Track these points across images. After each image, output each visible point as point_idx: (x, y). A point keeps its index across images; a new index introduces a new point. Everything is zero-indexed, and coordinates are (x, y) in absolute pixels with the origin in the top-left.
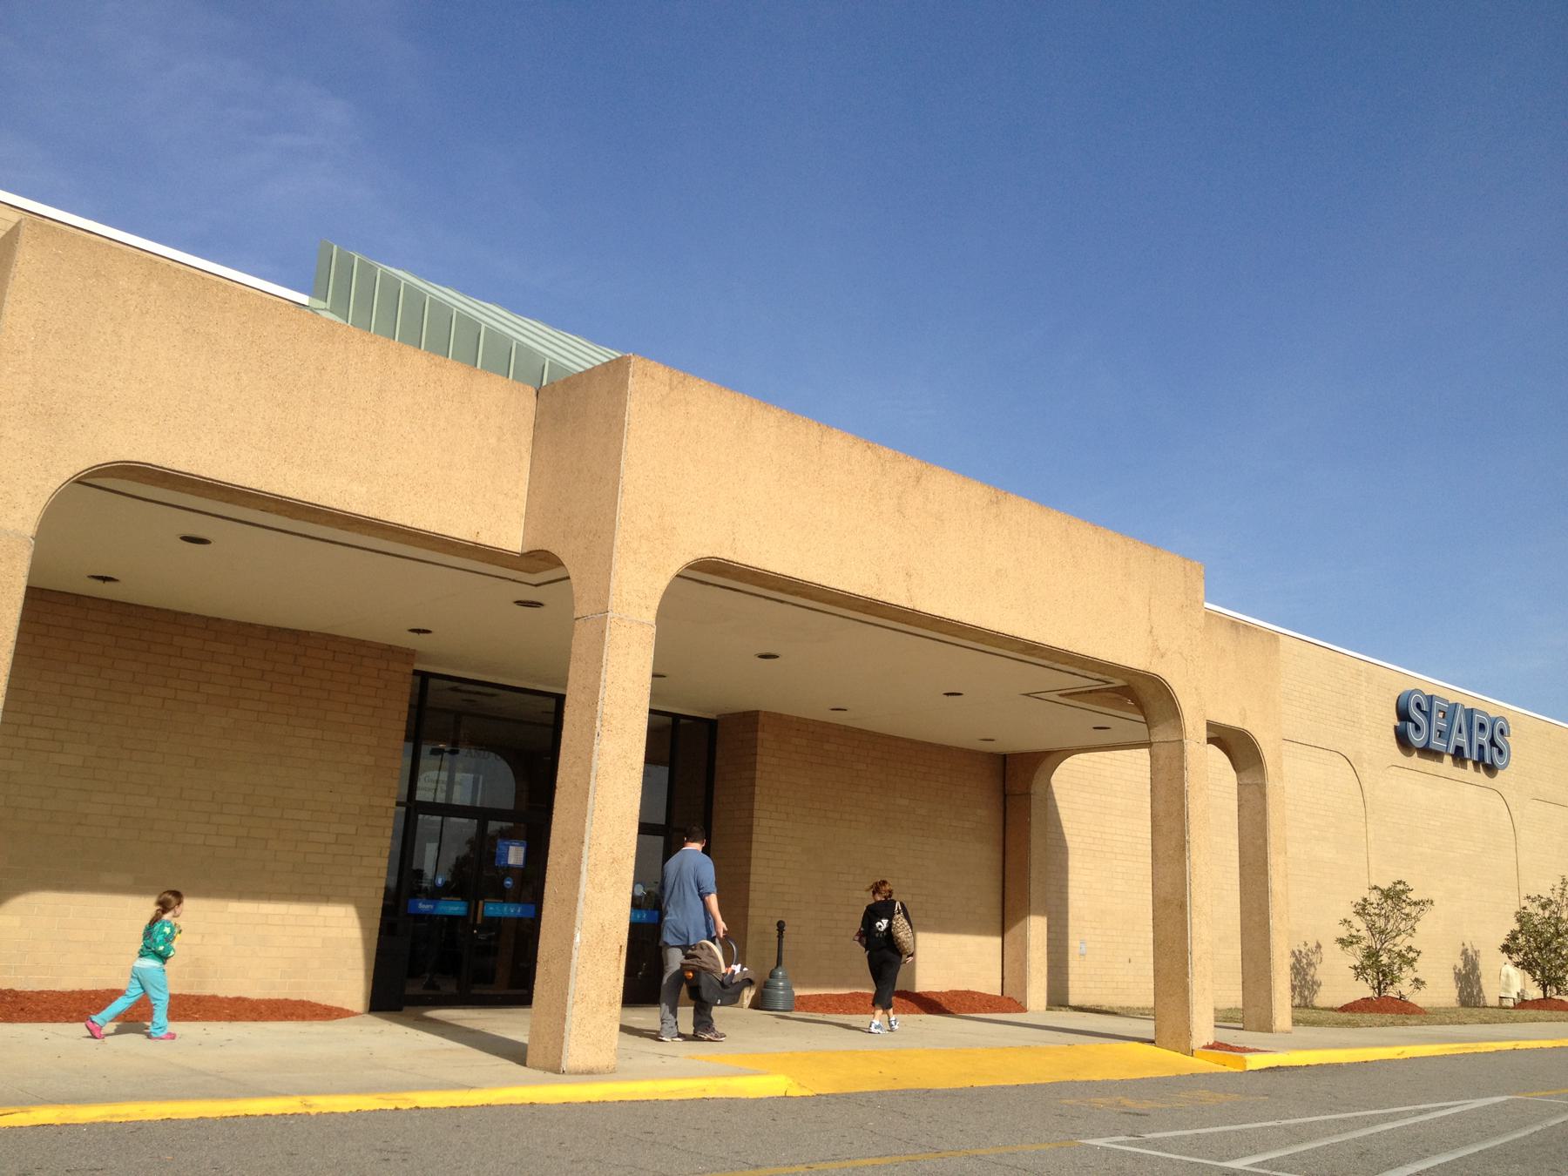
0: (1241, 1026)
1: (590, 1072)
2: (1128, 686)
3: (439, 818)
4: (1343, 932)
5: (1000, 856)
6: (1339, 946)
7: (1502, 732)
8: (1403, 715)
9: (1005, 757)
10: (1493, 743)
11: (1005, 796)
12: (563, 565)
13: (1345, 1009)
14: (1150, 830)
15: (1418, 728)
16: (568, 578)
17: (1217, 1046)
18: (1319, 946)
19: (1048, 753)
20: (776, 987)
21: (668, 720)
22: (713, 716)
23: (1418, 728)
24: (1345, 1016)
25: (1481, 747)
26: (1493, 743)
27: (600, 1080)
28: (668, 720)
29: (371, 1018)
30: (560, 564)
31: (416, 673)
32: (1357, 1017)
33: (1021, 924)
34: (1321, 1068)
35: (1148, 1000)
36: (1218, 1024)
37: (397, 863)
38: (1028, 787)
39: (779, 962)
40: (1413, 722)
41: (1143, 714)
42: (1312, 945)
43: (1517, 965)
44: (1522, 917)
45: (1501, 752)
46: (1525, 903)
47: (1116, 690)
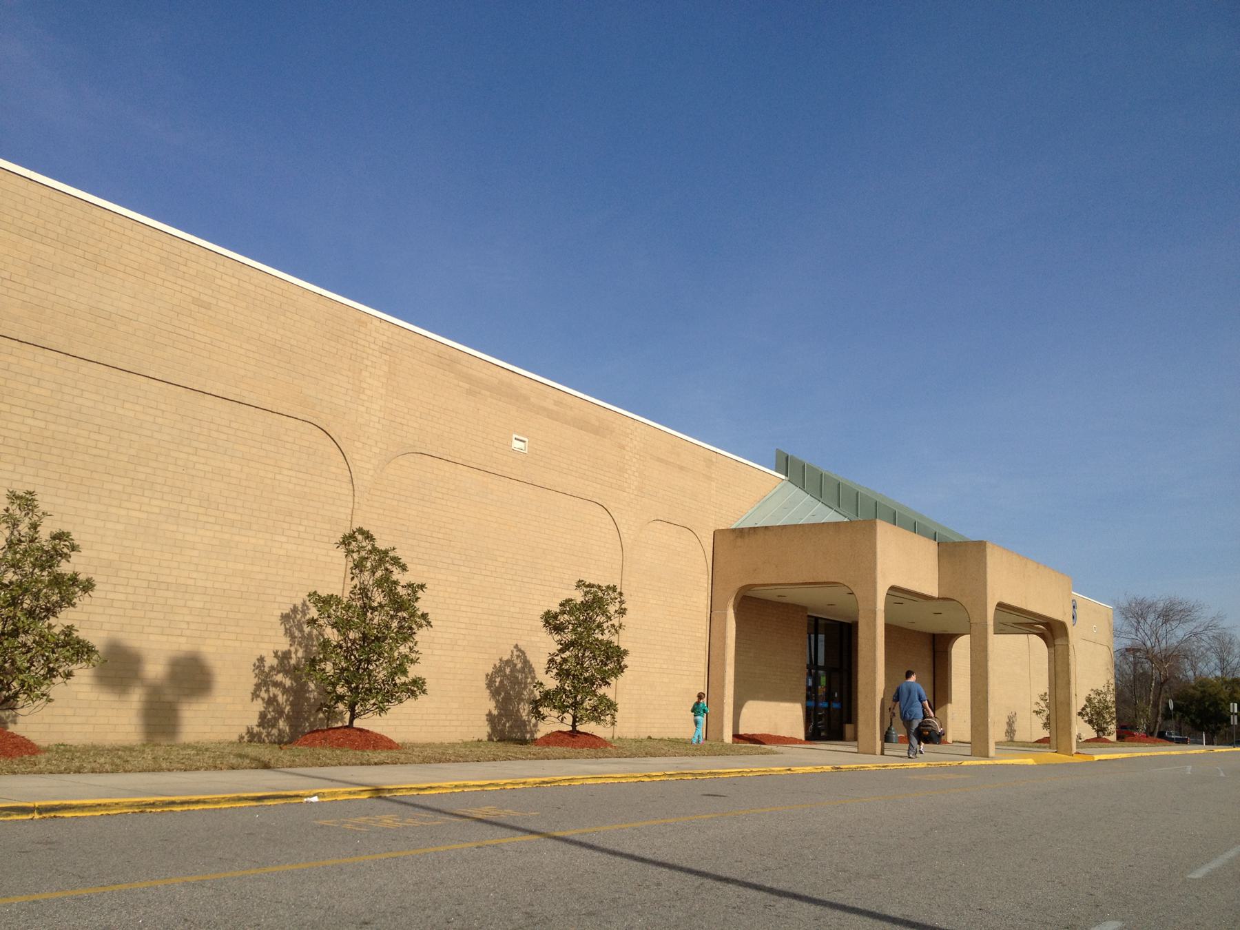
0: (856, 750)
4: (1036, 708)
5: (932, 678)
6: (493, 666)
9: (934, 635)
11: (934, 652)
13: (1037, 742)
17: (1077, 753)
18: (1015, 714)
20: (892, 734)
22: (850, 622)
24: (1038, 744)
29: (1120, 744)
31: (809, 616)
32: (1042, 745)
33: (944, 707)
34: (1114, 760)
35: (969, 739)
36: (997, 747)
37: (853, 697)
39: (891, 725)
42: (1014, 714)
43: (1086, 721)
44: (1089, 700)
46: (1091, 693)
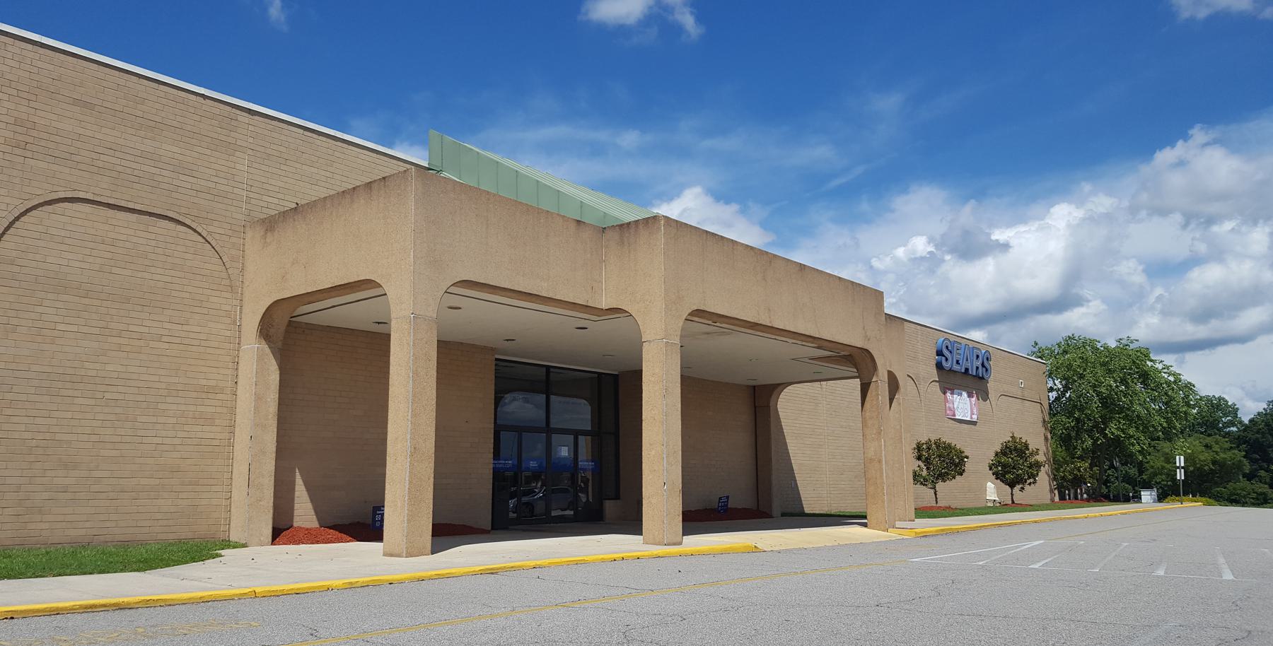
1: (926, 536)
2: (850, 355)
3: (1183, 465)
7: (987, 359)
8: (939, 353)
9: (754, 387)
10: (983, 365)
11: (755, 407)
12: (381, 286)
14: (493, 402)
15: (947, 359)
16: (386, 294)
19: (779, 385)
21: (596, 375)
23: (947, 359)
25: (977, 368)
26: (983, 365)
27: (524, 530)
28: (596, 375)
30: (380, 286)
38: (769, 403)
40: (944, 356)
41: (856, 366)
45: (987, 370)
47: (844, 357)
